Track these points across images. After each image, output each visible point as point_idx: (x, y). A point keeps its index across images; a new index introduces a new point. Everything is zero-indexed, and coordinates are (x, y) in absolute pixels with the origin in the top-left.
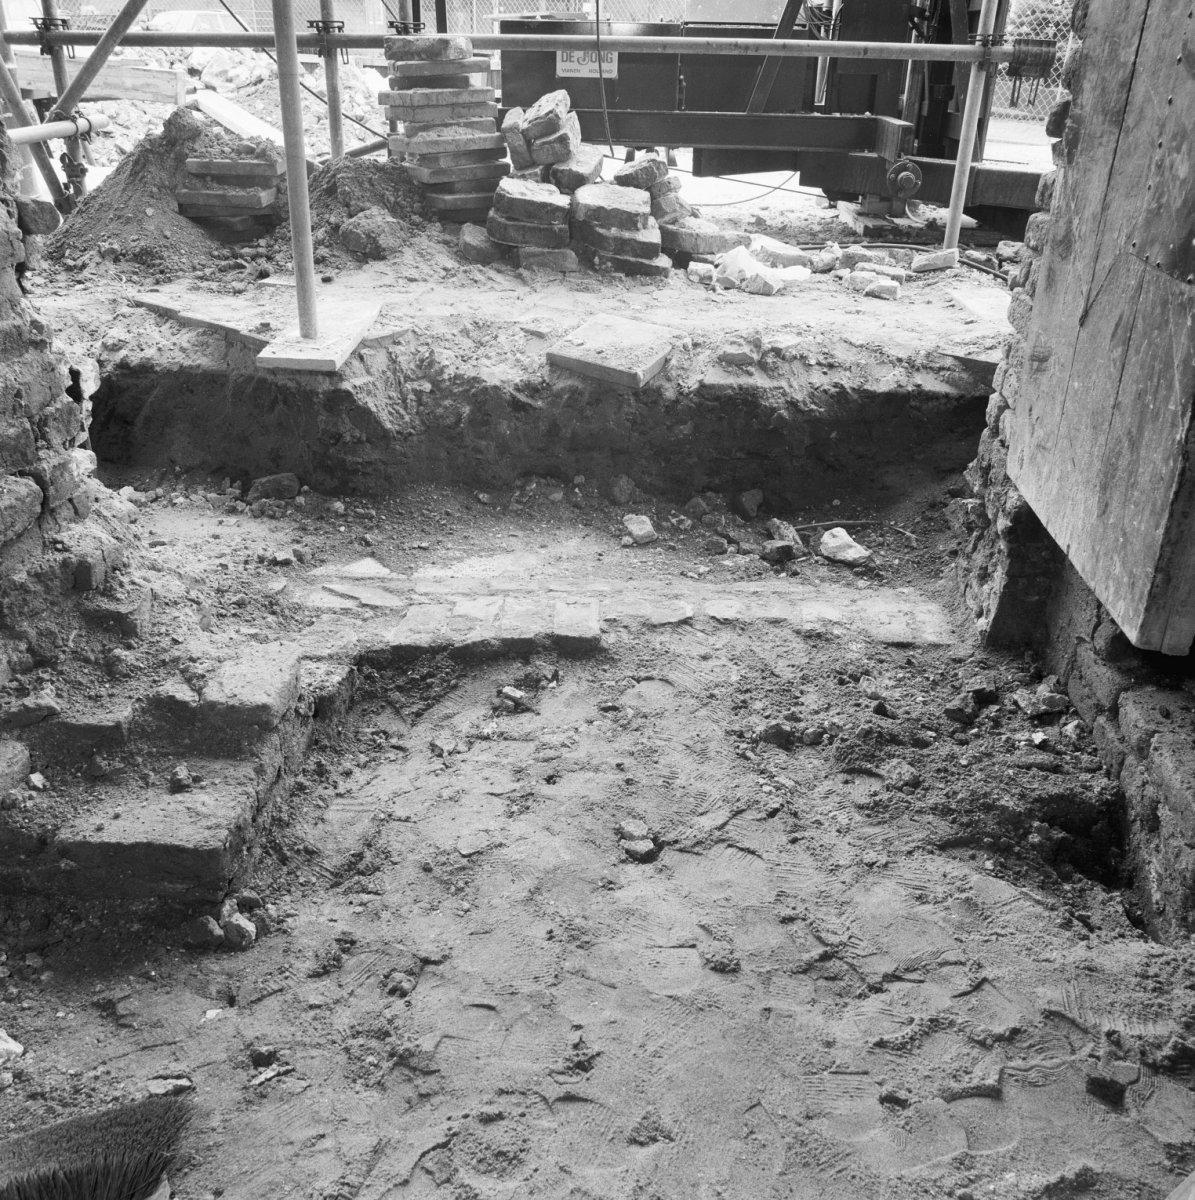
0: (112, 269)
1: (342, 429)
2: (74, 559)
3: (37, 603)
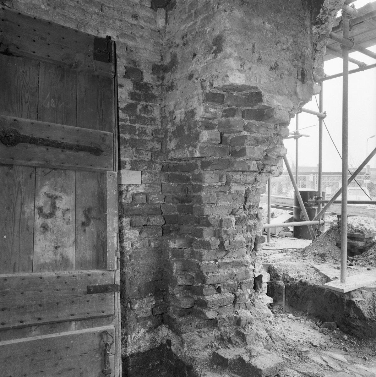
0: (313, 257)
1: (350, 313)
2: (238, 317)
3: (226, 324)
